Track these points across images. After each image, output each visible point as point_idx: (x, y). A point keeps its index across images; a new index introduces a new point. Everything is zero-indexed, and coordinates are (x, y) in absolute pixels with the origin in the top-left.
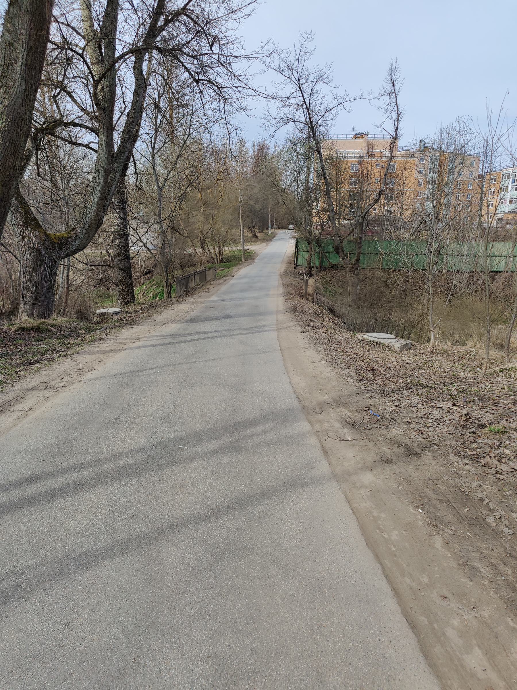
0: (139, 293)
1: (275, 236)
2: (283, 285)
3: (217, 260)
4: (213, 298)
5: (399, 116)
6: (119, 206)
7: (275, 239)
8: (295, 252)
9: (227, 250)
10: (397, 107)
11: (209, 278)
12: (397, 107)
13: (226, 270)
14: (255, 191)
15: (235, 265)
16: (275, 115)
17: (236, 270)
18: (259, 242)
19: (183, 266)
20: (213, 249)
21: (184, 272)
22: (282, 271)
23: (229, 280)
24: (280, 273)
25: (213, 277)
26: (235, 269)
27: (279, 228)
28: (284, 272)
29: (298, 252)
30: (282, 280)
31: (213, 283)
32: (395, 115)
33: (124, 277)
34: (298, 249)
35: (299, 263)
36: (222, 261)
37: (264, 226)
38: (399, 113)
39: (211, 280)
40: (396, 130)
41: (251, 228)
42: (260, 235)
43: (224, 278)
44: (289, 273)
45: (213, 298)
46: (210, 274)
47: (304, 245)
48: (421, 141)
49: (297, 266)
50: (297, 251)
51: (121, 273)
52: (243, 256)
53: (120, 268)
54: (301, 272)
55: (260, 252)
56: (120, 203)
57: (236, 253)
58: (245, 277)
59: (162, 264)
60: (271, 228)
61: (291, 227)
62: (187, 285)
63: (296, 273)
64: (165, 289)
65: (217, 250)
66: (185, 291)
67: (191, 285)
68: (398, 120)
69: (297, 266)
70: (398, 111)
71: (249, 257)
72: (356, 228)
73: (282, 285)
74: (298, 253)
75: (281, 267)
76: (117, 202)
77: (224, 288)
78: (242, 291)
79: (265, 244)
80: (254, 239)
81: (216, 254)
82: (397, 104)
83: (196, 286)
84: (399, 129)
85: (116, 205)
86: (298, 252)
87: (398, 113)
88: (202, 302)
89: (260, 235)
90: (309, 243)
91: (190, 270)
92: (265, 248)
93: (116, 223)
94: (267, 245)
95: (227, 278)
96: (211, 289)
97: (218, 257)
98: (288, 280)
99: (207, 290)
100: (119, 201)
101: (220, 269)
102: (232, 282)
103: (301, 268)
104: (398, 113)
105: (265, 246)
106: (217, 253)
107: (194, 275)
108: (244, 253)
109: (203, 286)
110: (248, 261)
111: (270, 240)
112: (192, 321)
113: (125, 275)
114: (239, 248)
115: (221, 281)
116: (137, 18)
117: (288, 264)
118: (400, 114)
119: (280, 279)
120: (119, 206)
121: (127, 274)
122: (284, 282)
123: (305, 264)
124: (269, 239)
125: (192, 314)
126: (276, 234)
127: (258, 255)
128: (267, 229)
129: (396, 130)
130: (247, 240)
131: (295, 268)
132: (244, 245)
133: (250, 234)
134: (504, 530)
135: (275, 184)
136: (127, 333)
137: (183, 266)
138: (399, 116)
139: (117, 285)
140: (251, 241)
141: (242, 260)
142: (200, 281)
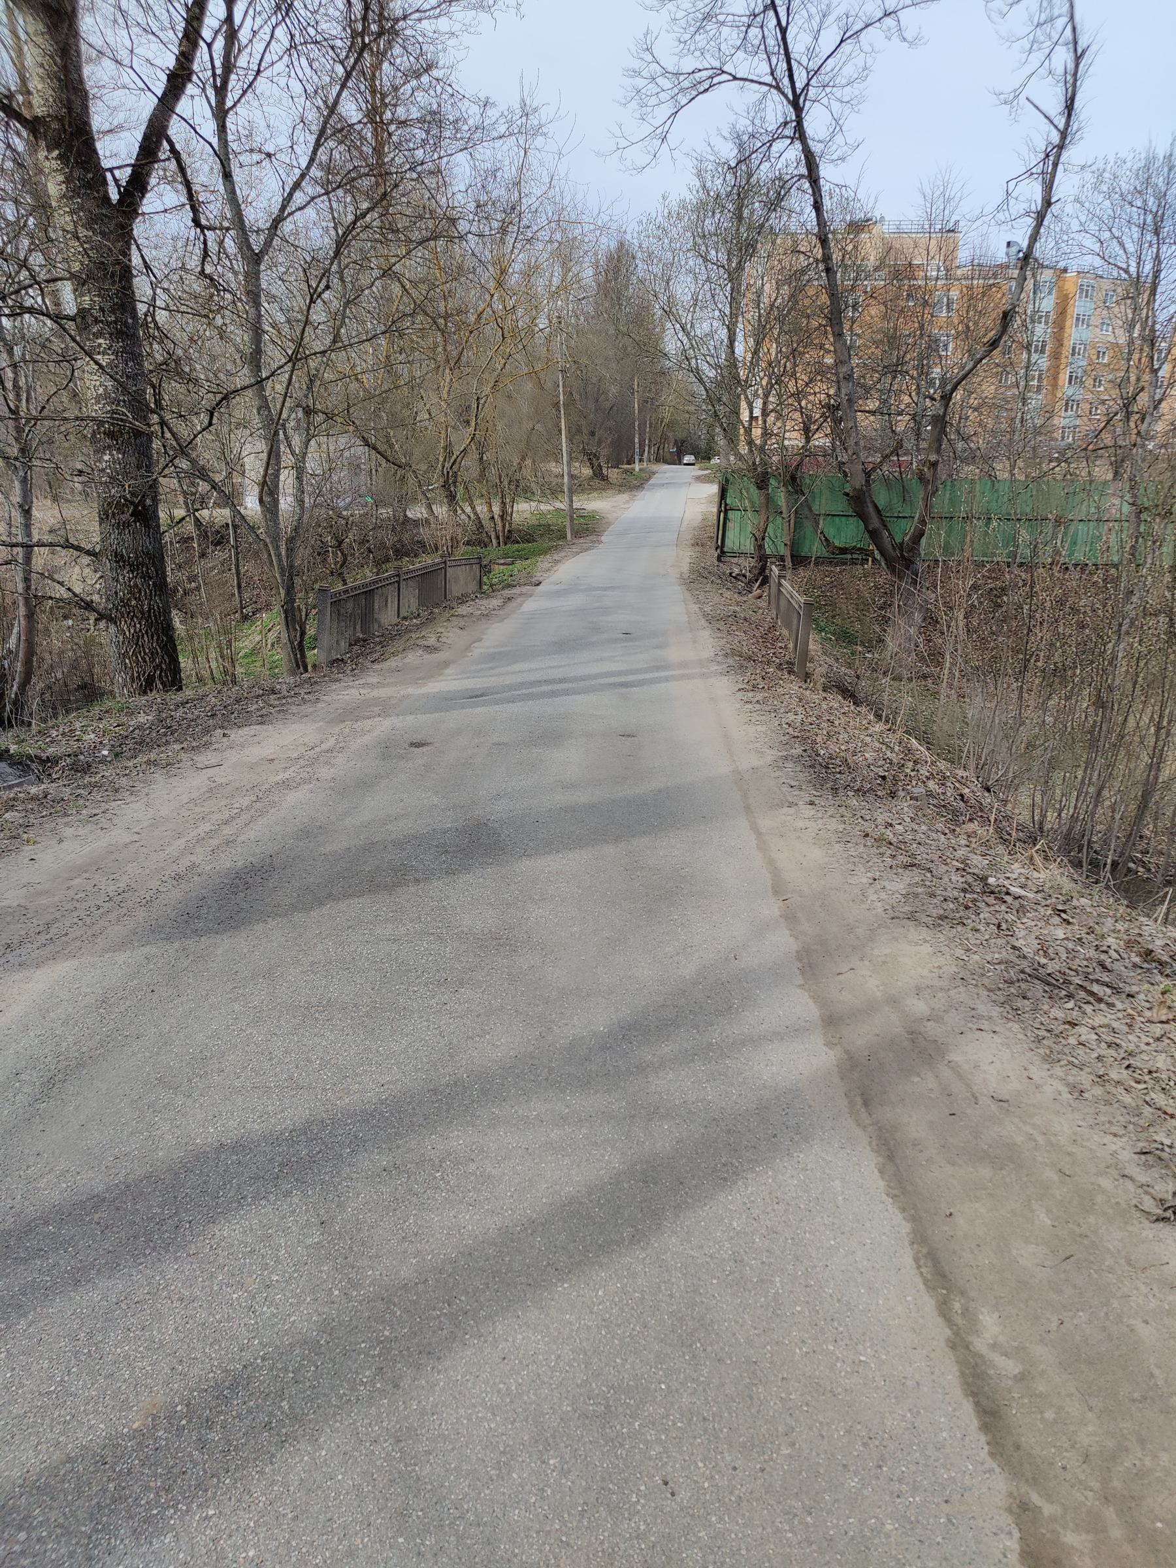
0: (269, 630)
1: (650, 478)
2: (710, 619)
3: (498, 538)
5: (1078, 59)
6: (109, 324)
7: (653, 485)
8: (720, 512)
9: (524, 511)
10: (1074, 29)
11: (456, 590)
12: (1074, 29)
13: (519, 564)
15: (545, 552)
16: (670, 65)
17: (546, 565)
18: (610, 492)
22: (685, 568)
23: (519, 600)
24: (681, 578)
25: (473, 587)
26: (544, 562)
27: (657, 460)
28: (692, 571)
29: (726, 511)
30: (698, 602)
31: (463, 610)
32: (1062, 57)
33: (133, 591)
34: (726, 505)
35: (729, 545)
36: (509, 538)
37: (622, 454)
38: (1080, 51)
39: (463, 600)
40: (1070, 106)
41: (591, 458)
42: (613, 474)
43: (507, 593)
44: (706, 574)
46: (461, 579)
47: (746, 494)
48: (1009, 244)
49: (723, 552)
50: (724, 508)
52: (568, 526)
54: (736, 571)
55: (615, 515)
56: (113, 312)
58: (572, 588)
59: (268, 540)
60: (641, 460)
61: (688, 459)
63: (724, 574)
65: (496, 509)
66: (357, 641)
67: (387, 617)
68: (1075, 74)
69: (723, 552)
70: (1075, 43)
72: (136, 743)
73: (703, 622)
74: (726, 514)
75: (682, 559)
76: (102, 309)
77: (496, 634)
78: (562, 646)
79: (625, 497)
80: (596, 482)
81: (493, 518)
82: (1072, 18)
83: (405, 618)
84: (1076, 105)
85: (96, 321)
86: (726, 511)
87: (1076, 50)
88: (386, 708)
90: (762, 483)
92: (627, 506)
93: (101, 391)
94: (632, 499)
95: (517, 590)
97: (499, 528)
98: (726, 599)
99: (432, 641)
100: (107, 305)
101: (502, 561)
102: (529, 606)
103: (735, 560)
104: (1076, 50)
105: (627, 502)
106: (496, 517)
107: (398, 582)
108: (572, 517)
110: (581, 540)
111: (639, 487)
113: (139, 581)
114: (559, 505)
115: (495, 602)
117: (698, 549)
118: (1084, 52)
119: (688, 595)
120: (109, 324)
121: (146, 577)
122: (708, 609)
123: (749, 546)
124: (635, 484)
126: (654, 473)
127: (609, 524)
128: (630, 461)
129: (1070, 106)
130: (578, 487)
131: (719, 559)
133: (587, 472)
135: (650, 348)
138: (1078, 59)
139: (111, 620)
140: (593, 489)
141: (565, 537)
142: (422, 603)
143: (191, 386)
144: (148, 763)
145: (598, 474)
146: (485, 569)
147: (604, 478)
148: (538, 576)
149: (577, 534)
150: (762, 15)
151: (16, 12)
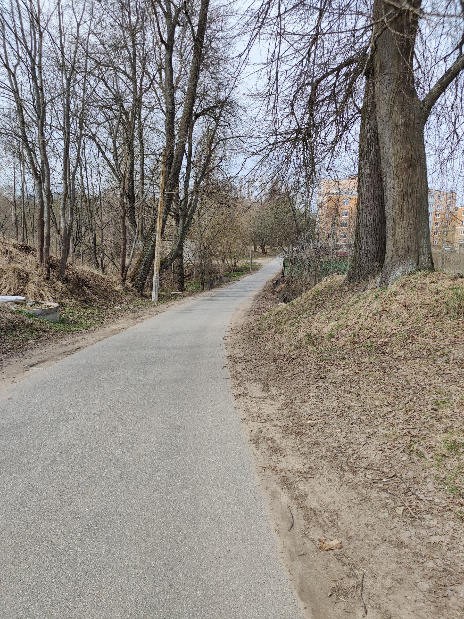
4: (224, 290)
9: (241, 263)
14: (379, 78)
19: (210, 273)
20: (230, 262)
21: (211, 277)
25: (228, 280)
26: (242, 276)
36: (236, 270)
39: (226, 282)
45: (224, 290)
46: (225, 279)
50: (284, 267)
51: (179, 276)
53: (178, 274)
57: (247, 265)
58: (246, 281)
62: (212, 284)
64: (201, 285)
67: (215, 284)
71: (255, 268)
78: (240, 288)
79: (271, 259)
80: (263, 255)
89: (269, 252)
91: (214, 276)
96: (224, 286)
102: (237, 284)
109: (221, 285)
112: (213, 297)
116: (391, 476)
125: (213, 295)
127: (262, 267)
130: (258, 256)
132: (251, 260)
134: (313, 330)
136: (189, 298)
137: (210, 273)
143: (414, 457)
144: (396, 205)
145: (264, 252)
146: (230, 277)
147: (265, 253)
148: (240, 279)
149: (252, 270)
150: (256, 27)
151: (126, 266)
